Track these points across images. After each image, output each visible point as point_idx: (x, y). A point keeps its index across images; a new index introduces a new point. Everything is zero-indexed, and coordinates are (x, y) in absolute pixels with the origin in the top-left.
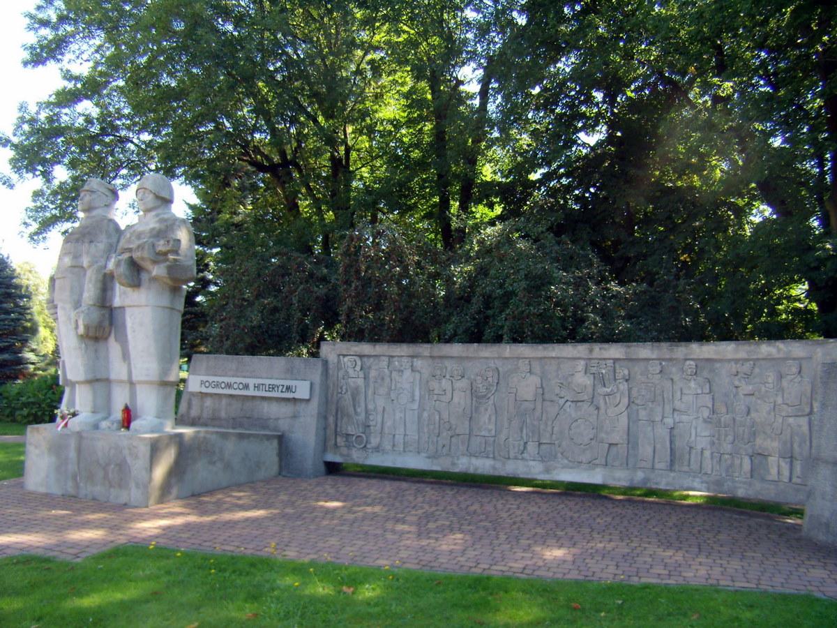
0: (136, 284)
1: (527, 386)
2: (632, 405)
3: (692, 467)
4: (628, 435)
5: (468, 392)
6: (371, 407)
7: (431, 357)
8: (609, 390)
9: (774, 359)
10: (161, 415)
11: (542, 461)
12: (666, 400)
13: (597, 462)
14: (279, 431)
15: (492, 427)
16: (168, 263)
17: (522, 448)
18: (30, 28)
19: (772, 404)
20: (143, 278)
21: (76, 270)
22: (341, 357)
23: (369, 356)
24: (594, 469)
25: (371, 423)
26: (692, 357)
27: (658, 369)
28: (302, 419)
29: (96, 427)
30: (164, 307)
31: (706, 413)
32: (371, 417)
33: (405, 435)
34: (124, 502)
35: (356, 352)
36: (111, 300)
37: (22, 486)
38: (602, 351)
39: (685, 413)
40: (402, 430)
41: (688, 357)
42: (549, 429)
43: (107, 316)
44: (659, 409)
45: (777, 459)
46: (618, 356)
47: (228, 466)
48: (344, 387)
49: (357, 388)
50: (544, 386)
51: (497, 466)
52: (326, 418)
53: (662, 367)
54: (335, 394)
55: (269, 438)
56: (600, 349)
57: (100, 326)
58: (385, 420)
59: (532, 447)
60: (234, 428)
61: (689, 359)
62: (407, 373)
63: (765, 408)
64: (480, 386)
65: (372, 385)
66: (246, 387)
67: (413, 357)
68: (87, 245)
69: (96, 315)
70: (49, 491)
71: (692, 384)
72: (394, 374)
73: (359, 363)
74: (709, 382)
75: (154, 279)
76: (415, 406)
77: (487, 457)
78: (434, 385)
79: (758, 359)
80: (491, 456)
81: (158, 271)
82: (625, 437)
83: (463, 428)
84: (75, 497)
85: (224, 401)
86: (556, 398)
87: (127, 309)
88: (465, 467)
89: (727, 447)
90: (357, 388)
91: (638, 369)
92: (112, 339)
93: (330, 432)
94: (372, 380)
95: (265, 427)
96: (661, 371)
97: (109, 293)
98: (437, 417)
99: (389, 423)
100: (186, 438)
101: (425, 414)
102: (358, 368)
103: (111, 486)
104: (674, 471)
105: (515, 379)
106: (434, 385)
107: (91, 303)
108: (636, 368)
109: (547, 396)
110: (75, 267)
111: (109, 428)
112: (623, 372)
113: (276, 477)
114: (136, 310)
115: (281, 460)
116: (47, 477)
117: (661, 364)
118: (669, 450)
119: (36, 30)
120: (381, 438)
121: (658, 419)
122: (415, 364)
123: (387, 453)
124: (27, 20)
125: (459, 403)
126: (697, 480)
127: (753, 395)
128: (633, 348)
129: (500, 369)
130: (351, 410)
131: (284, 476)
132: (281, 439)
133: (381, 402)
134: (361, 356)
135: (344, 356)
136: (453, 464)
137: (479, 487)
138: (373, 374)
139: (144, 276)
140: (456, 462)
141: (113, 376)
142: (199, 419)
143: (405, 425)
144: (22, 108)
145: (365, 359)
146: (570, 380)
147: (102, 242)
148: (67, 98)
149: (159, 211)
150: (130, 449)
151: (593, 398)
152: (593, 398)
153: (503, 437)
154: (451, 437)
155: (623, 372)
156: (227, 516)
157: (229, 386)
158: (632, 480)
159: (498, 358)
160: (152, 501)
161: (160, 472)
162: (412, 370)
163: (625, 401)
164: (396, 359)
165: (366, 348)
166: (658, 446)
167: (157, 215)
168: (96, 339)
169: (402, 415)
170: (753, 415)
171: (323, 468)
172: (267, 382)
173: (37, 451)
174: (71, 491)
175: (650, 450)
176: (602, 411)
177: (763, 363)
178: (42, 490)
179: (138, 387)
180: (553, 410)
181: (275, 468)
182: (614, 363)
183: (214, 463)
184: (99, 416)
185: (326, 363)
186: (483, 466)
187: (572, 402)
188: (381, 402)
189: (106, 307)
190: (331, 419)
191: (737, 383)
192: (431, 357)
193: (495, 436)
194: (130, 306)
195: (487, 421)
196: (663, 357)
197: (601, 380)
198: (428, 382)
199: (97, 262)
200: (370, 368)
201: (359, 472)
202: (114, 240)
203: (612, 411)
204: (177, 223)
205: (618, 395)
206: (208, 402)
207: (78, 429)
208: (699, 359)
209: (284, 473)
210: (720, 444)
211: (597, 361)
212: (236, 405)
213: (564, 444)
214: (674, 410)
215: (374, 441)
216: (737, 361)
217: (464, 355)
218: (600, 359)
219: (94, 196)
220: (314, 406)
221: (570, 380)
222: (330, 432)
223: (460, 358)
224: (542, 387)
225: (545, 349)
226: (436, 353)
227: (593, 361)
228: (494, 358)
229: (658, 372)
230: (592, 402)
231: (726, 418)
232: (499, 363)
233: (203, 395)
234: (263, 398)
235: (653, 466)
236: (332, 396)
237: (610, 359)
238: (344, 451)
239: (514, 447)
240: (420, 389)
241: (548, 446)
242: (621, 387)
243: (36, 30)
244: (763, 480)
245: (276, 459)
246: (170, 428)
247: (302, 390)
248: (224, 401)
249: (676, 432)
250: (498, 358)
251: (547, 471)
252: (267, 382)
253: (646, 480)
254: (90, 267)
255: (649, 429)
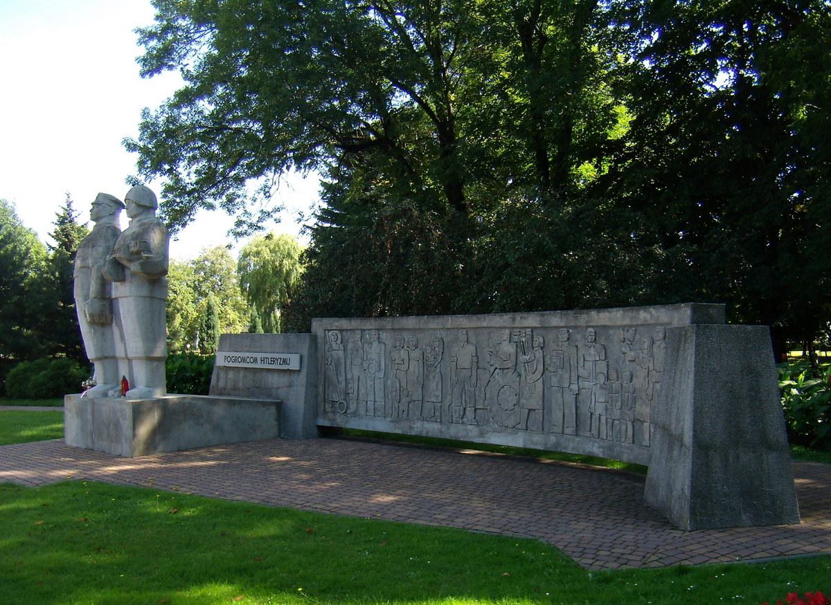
0: (122, 280)
1: (465, 356)
2: (546, 372)
3: (593, 432)
4: (543, 401)
5: (421, 361)
6: (349, 376)
7: (392, 329)
8: (528, 357)
9: (649, 325)
10: (151, 384)
11: (478, 425)
12: (572, 367)
13: (519, 426)
14: (279, 399)
15: (439, 393)
16: (142, 261)
17: (462, 413)
18: (140, 42)
19: (647, 370)
20: (126, 273)
21: (84, 270)
22: (327, 332)
23: (347, 330)
24: (517, 433)
25: (349, 391)
26: (592, 324)
27: (566, 336)
28: (295, 388)
29: (105, 395)
30: (144, 297)
31: (602, 379)
32: (350, 386)
33: (375, 401)
34: (118, 454)
35: (336, 326)
36: (110, 293)
37: (64, 442)
38: (523, 319)
39: (586, 379)
40: (373, 397)
41: (590, 324)
42: (483, 395)
43: (107, 306)
44: (567, 376)
45: (648, 424)
46: (535, 324)
47: (217, 427)
48: (329, 360)
49: (339, 359)
50: (478, 354)
51: (443, 430)
52: (316, 387)
53: (569, 335)
54: (323, 365)
55: (271, 403)
56: (521, 318)
57: (101, 314)
58: (360, 388)
59: (470, 413)
60: (248, 397)
61: (590, 327)
62: (375, 344)
63: (642, 373)
64: (430, 355)
65: (349, 356)
66: (255, 360)
67: (379, 330)
68: (90, 249)
69: (98, 305)
70: (78, 446)
71: (592, 351)
72: (365, 345)
73: (340, 337)
74: (605, 348)
75: (134, 274)
76: (382, 375)
77: (436, 422)
78: (395, 355)
79: (637, 325)
80: (439, 420)
81: (134, 267)
82: (541, 403)
83: (417, 395)
84: (92, 450)
85: (242, 374)
86: (488, 366)
87: (119, 299)
88: (419, 430)
89: (617, 413)
90: (339, 359)
91: (550, 336)
92: (114, 324)
93: (320, 398)
94: (349, 352)
95: (269, 396)
96: (568, 339)
97: (108, 287)
98: (398, 385)
99: (362, 391)
100: (170, 404)
101: (389, 382)
102: (339, 342)
103: (112, 441)
104: (579, 436)
105: (456, 349)
106: (395, 355)
107: (94, 296)
108: (550, 337)
109: (480, 365)
110: (83, 267)
111: (113, 395)
112: (539, 340)
113: (275, 438)
114: (124, 299)
115: (279, 425)
116: (77, 434)
117: (568, 331)
118: (575, 415)
119: (146, 43)
120: (357, 404)
121: (566, 385)
122: (381, 336)
123: (362, 417)
124: (138, 36)
125: (414, 372)
126: (596, 445)
127: (634, 361)
128: (546, 317)
129: (445, 340)
130: (335, 379)
131: (282, 438)
132: (280, 406)
133: (356, 372)
134: (341, 331)
135: (329, 330)
136: (411, 428)
137: (437, 450)
138: (350, 346)
139: (127, 273)
140: (412, 425)
141: (118, 355)
142: (224, 389)
143: (375, 394)
144: (145, 113)
145: (344, 333)
146: (497, 349)
147: (101, 246)
148: (185, 98)
149: (142, 217)
150: (121, 412)
151: (516, 365)
152: (516, 365)
153: (447, 402)
154: (409, 403)
155: (539, 340)
156: (180, 465)
157: (244, 360)
158: (546, 444)
159: (442, 329)
160: (137, 453)
161: (144, 430)
162: (379, 342)
163: (541, 367)
164: (367, 332)
165: (344, 323)
166: (566, 412)
167: (139, 221)
168: (103, 325)
169: (372, 383)
170: (635, 380)
171: (315, 431)
172: (270, 356)
173: (70, 415)
174: (90, 445)
175: (560, 415)
176: (523, 377)
177: (641, 328)
178: (74, 445)
179: (134, 361)
180: (486, 377)
181: (274, 431)
182: (532, 332)
183: (202, 424)
184: (108, 387)
185: (314, 339)
186: (431, 429)
187: (500, 369)
188: (356, 372)
189: (105, 299)
190: (321, 388)
191: (623, 349)
192: (392, 329)
193: (441, 402)
194: (121, 297)
195: (435, 388)
196: (569, 325)
197: (522, 348)
198: (390, 352)
199: (97, 263)
200: (348, 341)
201: (360, 436)
202: (112, 243)
203: (531, 378)
204: (151, 227)
205: (535, 363)
206: (231, 375)
207: (92, 397)
208: (597, 326)
209: (282, 435)
210: (612, 409)
211: (519, 330)
212: (250, 376)
213: (494, 409)
214: (578, 377)
215: (353, 407)
216: (624, 327)
217: (417, 327)
218: (521, 328)
219: (100, 208)
220: (302, 379)
221: (497, 349)
222: (320, 398)
223: (414, 330)
224: (477, 356)
225: (479, 319)
226: (396, 327)
227: (515, 330)
228: (439, 329)
229: (566, 339)
230: (516, 370)
231: (616, 385)
232: (444, 333)
233: (227, 369)
234: (268, 370)
235: (563, 431)
236: (321, 368)
237: (528, 328)
238: (330, 415)
239: (456, 412)
240: (385, 359)
241: (482, 410)
242: (537, 355)
243: (146, 43)
244: (641, 445)
245: (274, 423)
246: (160, 394)
247: (294, 364)
248: (242, 374)
249: (580, 398)
250: (442, 329)
251: (482, 434)
252: (270, 356)
253: (558, 444)
254: (93, 266)
255: (560, 394)
